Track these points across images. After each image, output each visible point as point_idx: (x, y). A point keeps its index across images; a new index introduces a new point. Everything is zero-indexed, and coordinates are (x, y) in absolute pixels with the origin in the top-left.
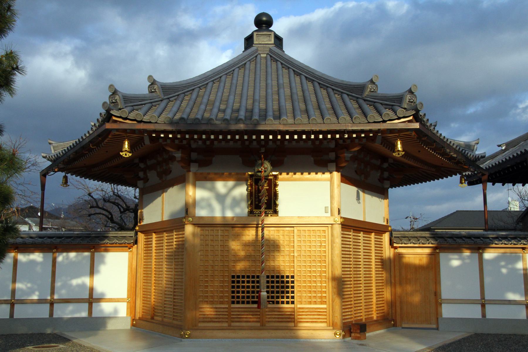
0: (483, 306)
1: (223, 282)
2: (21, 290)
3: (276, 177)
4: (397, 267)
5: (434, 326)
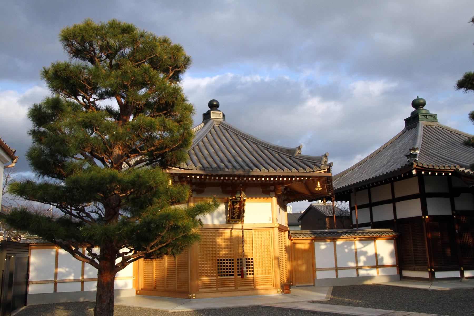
0: (337, 271)
1: (213, 264)
2: (60, 272)
3: (244, 200)
4: (293, 252)
5: (312, 284)
